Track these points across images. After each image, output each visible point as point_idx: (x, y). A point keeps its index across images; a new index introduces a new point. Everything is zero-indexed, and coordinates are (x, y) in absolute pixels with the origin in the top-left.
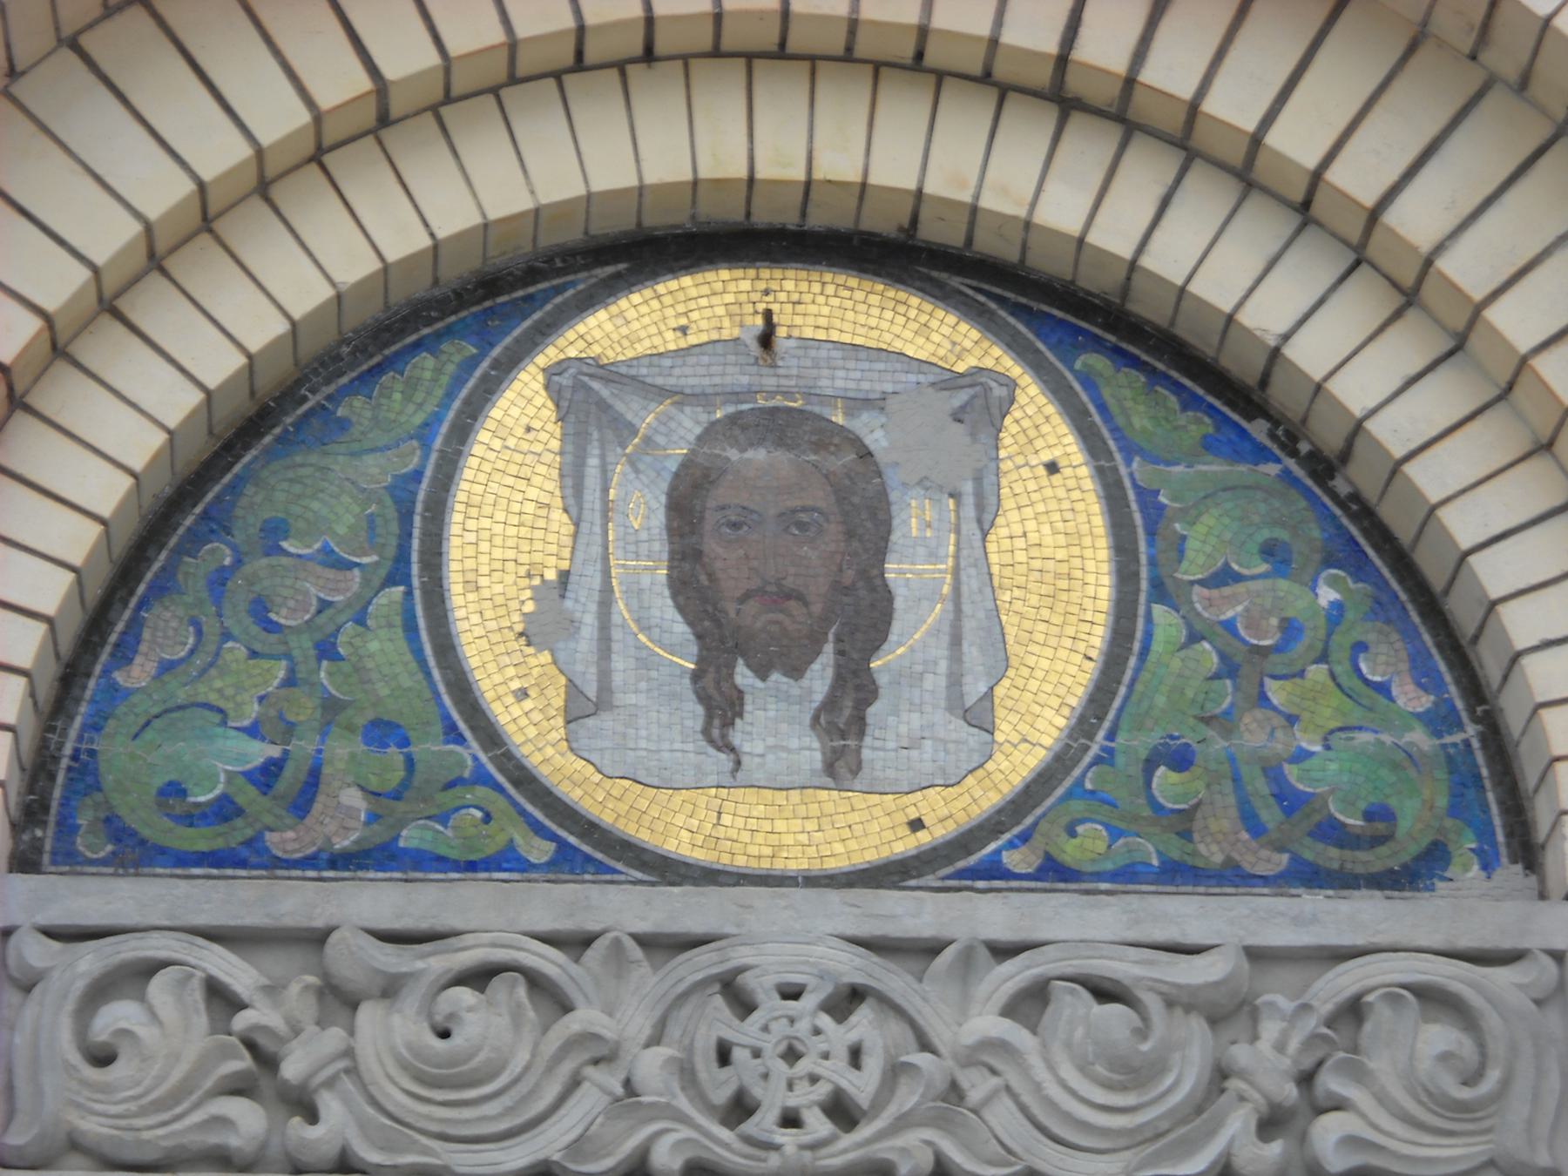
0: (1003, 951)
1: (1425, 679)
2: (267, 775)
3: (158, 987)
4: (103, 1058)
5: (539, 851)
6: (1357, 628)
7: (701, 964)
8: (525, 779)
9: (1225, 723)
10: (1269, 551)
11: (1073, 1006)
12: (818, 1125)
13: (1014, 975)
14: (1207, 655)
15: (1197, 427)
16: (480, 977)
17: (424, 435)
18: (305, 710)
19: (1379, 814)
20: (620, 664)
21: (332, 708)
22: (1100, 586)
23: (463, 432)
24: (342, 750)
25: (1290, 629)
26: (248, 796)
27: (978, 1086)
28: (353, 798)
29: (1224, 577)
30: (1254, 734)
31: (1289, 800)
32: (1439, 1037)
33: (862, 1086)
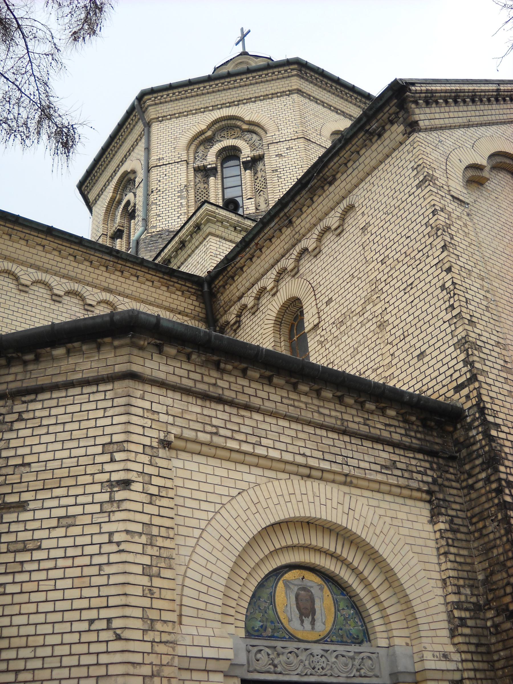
0: (335, 651)
1: (361, 622)
2: (262, 626)
3: (262, 652)
4: (258, 660)
5: (287, 637)
6: (355, 616)
7: (309, 652)
8: (285, 628)
9: (345, 625)
10: (347, 606)
11: (340, 658)
12: (321, 670)
13: (335, 654)
14: (343, 618)
15: (340, 592)
16: (290, 653)
17: (272, 587)
18: (264, 619)
19: (358, 636)
20: (293, 616)
21: (267, 619)
22: (333, 610)
23: (276, 587)
24: (269, 624)
25: (349, 615)
26: (260, 629)
27: (334, 666)
28: (270, 630)
29: (343, 609)
30: (347, 627)
31: (351, 634)
32: (370, 662)
33: (324, 665)
